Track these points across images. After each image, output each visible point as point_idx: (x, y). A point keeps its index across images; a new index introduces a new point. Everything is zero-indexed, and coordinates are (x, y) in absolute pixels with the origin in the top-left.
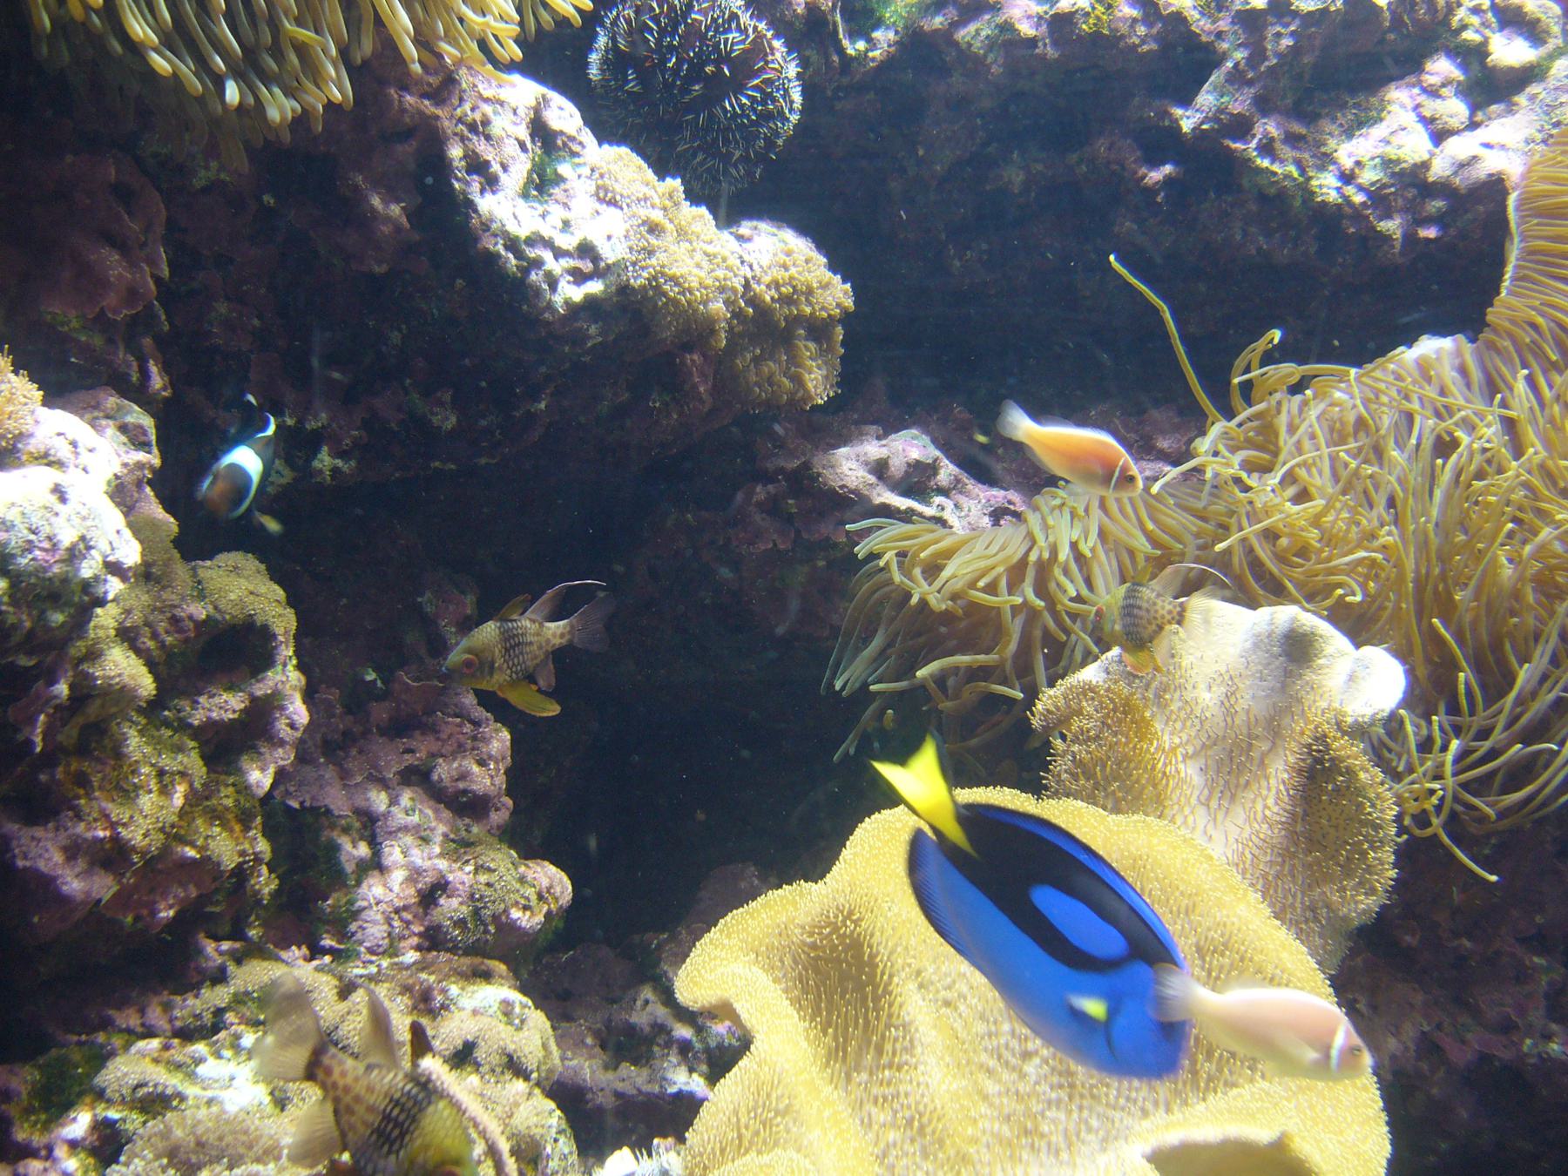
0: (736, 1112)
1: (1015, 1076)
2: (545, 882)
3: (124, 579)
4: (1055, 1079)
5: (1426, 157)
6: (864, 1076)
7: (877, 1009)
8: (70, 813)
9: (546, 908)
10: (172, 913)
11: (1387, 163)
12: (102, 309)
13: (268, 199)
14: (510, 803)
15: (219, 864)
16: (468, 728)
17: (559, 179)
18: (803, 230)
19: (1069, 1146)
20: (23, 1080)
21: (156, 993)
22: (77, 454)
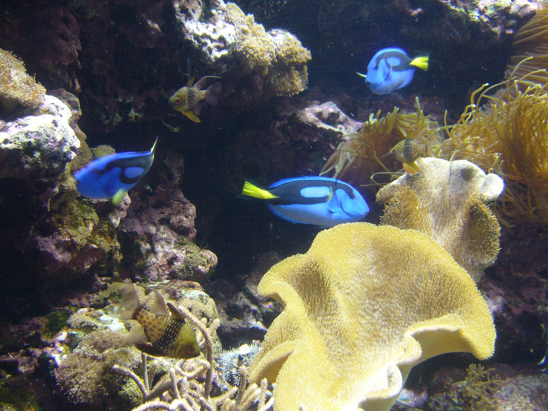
0: (281, 329)
1: (371, 317)
2: (209, 257)
3: (76, 152)
4: (384, 318)
5: (509, 5)
6: (321, 318)
7: (324, 296)
8: (57, 233)
9: (209, 265)
10: (89, 267)
11: (496, 7)
12: (61, 62)
13: (112, 23)
14: (196, 230)
15: (104, 250)
16: (181, 205)
17: (212, 15)
18: (292, 33)
19: (389, 340)
20: (43, 321)
21: (83, 293)
22: (58, 110)
